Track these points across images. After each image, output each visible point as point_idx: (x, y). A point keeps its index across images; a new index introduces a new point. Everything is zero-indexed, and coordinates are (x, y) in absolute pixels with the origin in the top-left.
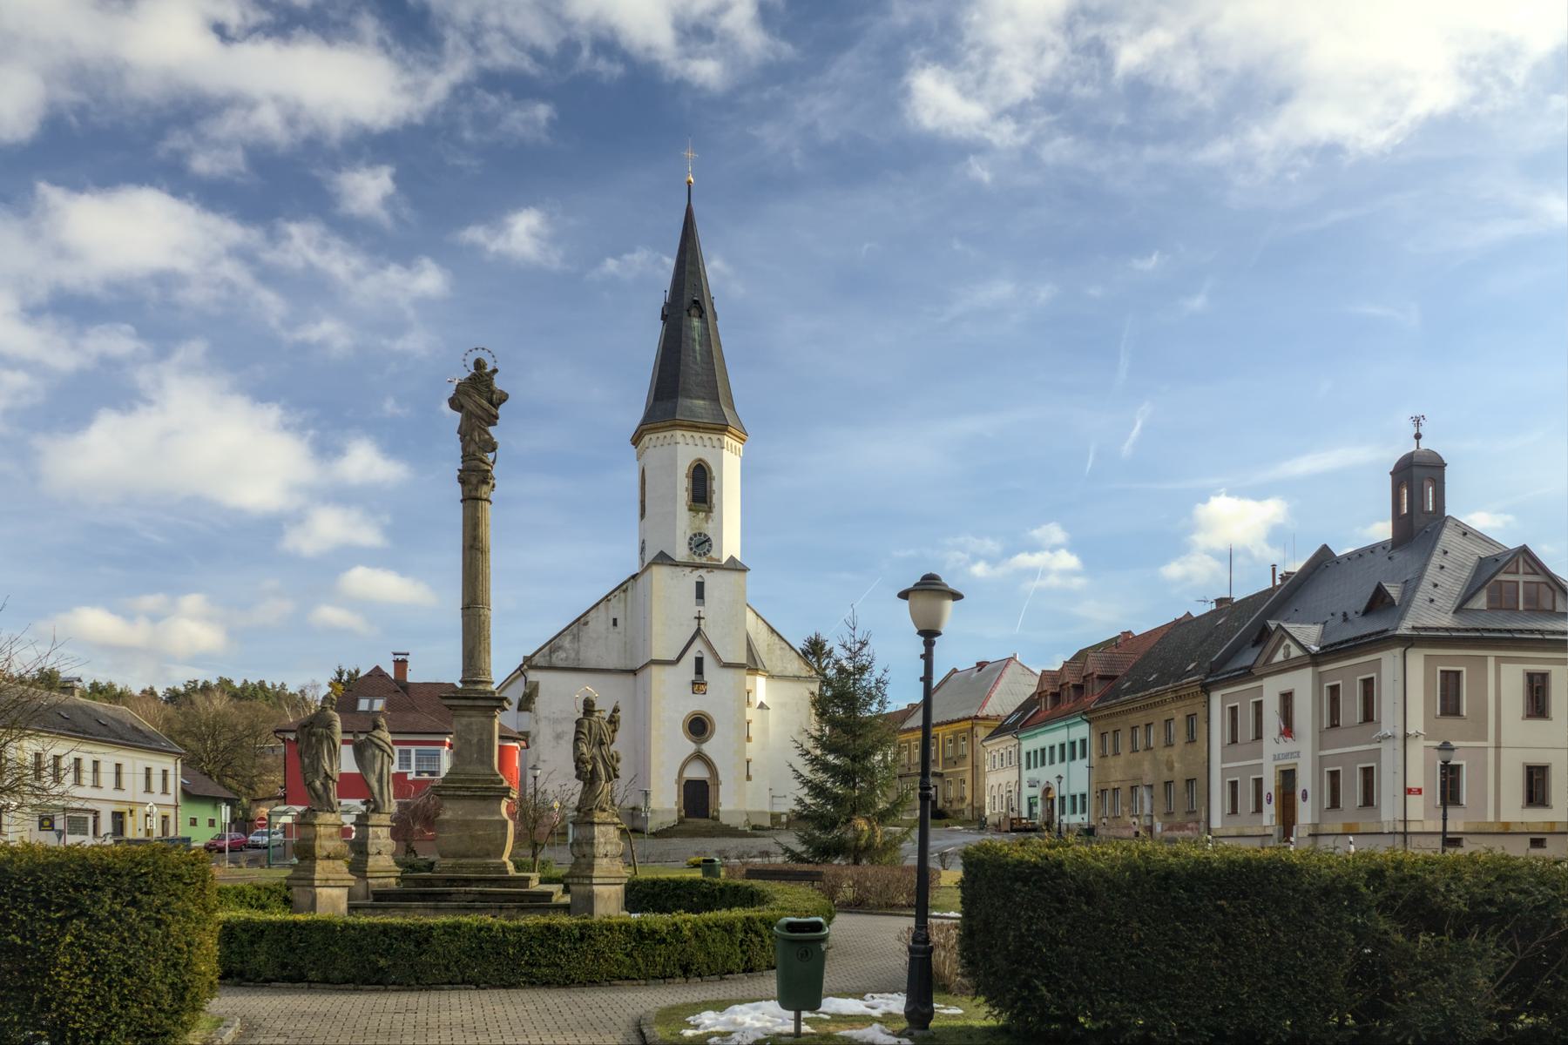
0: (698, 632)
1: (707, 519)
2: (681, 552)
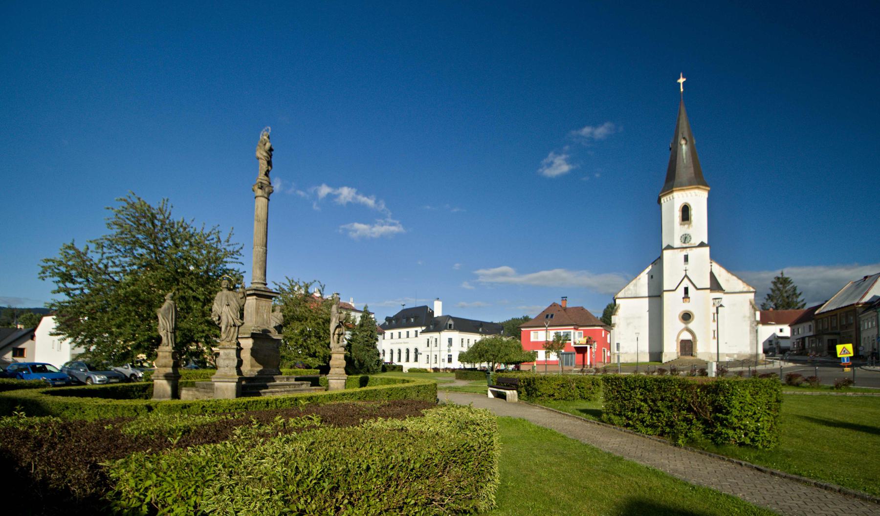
0: (686, 276)
2: (677, 243)
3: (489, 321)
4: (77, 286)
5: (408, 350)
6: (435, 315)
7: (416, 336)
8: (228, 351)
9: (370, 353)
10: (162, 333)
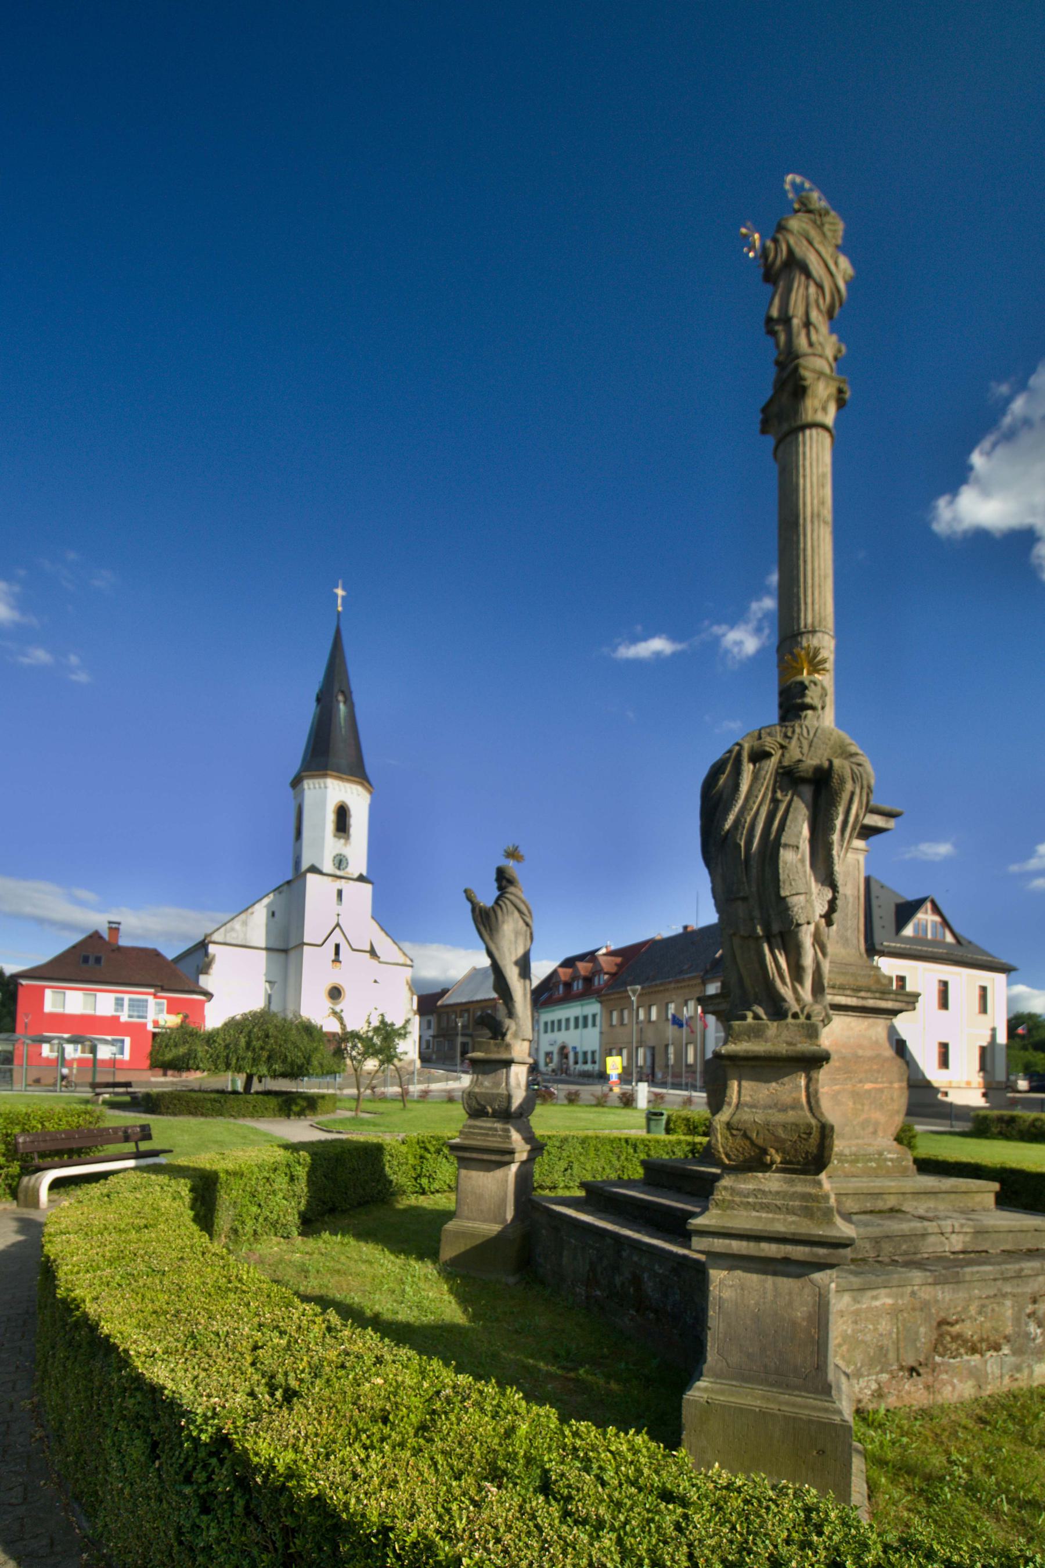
0: (338, 925)
1: (345, 844)
2: (328, 867)
3: (676, 929)
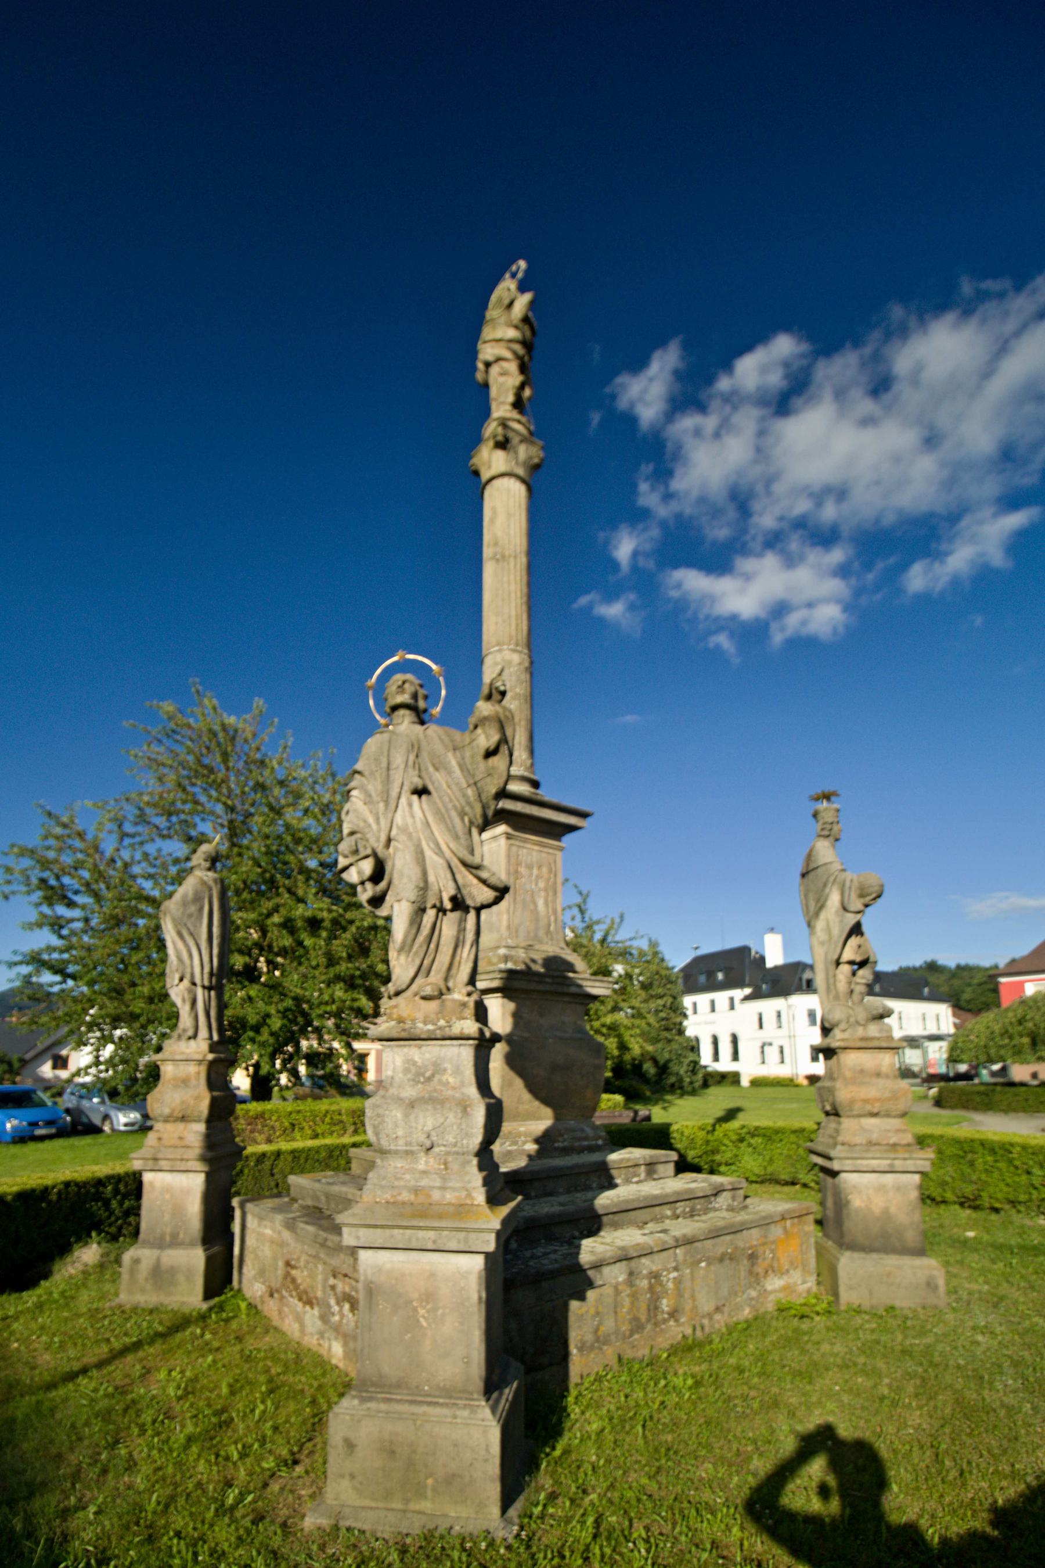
4: (76, 913)
5: (715, 1041)
6: (769, 964)
7: (732, 1007)
8: (431, 1052)
9: (675, 1046)
10: (177, 993)
